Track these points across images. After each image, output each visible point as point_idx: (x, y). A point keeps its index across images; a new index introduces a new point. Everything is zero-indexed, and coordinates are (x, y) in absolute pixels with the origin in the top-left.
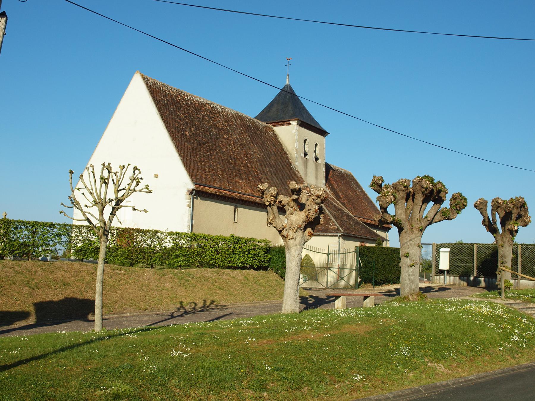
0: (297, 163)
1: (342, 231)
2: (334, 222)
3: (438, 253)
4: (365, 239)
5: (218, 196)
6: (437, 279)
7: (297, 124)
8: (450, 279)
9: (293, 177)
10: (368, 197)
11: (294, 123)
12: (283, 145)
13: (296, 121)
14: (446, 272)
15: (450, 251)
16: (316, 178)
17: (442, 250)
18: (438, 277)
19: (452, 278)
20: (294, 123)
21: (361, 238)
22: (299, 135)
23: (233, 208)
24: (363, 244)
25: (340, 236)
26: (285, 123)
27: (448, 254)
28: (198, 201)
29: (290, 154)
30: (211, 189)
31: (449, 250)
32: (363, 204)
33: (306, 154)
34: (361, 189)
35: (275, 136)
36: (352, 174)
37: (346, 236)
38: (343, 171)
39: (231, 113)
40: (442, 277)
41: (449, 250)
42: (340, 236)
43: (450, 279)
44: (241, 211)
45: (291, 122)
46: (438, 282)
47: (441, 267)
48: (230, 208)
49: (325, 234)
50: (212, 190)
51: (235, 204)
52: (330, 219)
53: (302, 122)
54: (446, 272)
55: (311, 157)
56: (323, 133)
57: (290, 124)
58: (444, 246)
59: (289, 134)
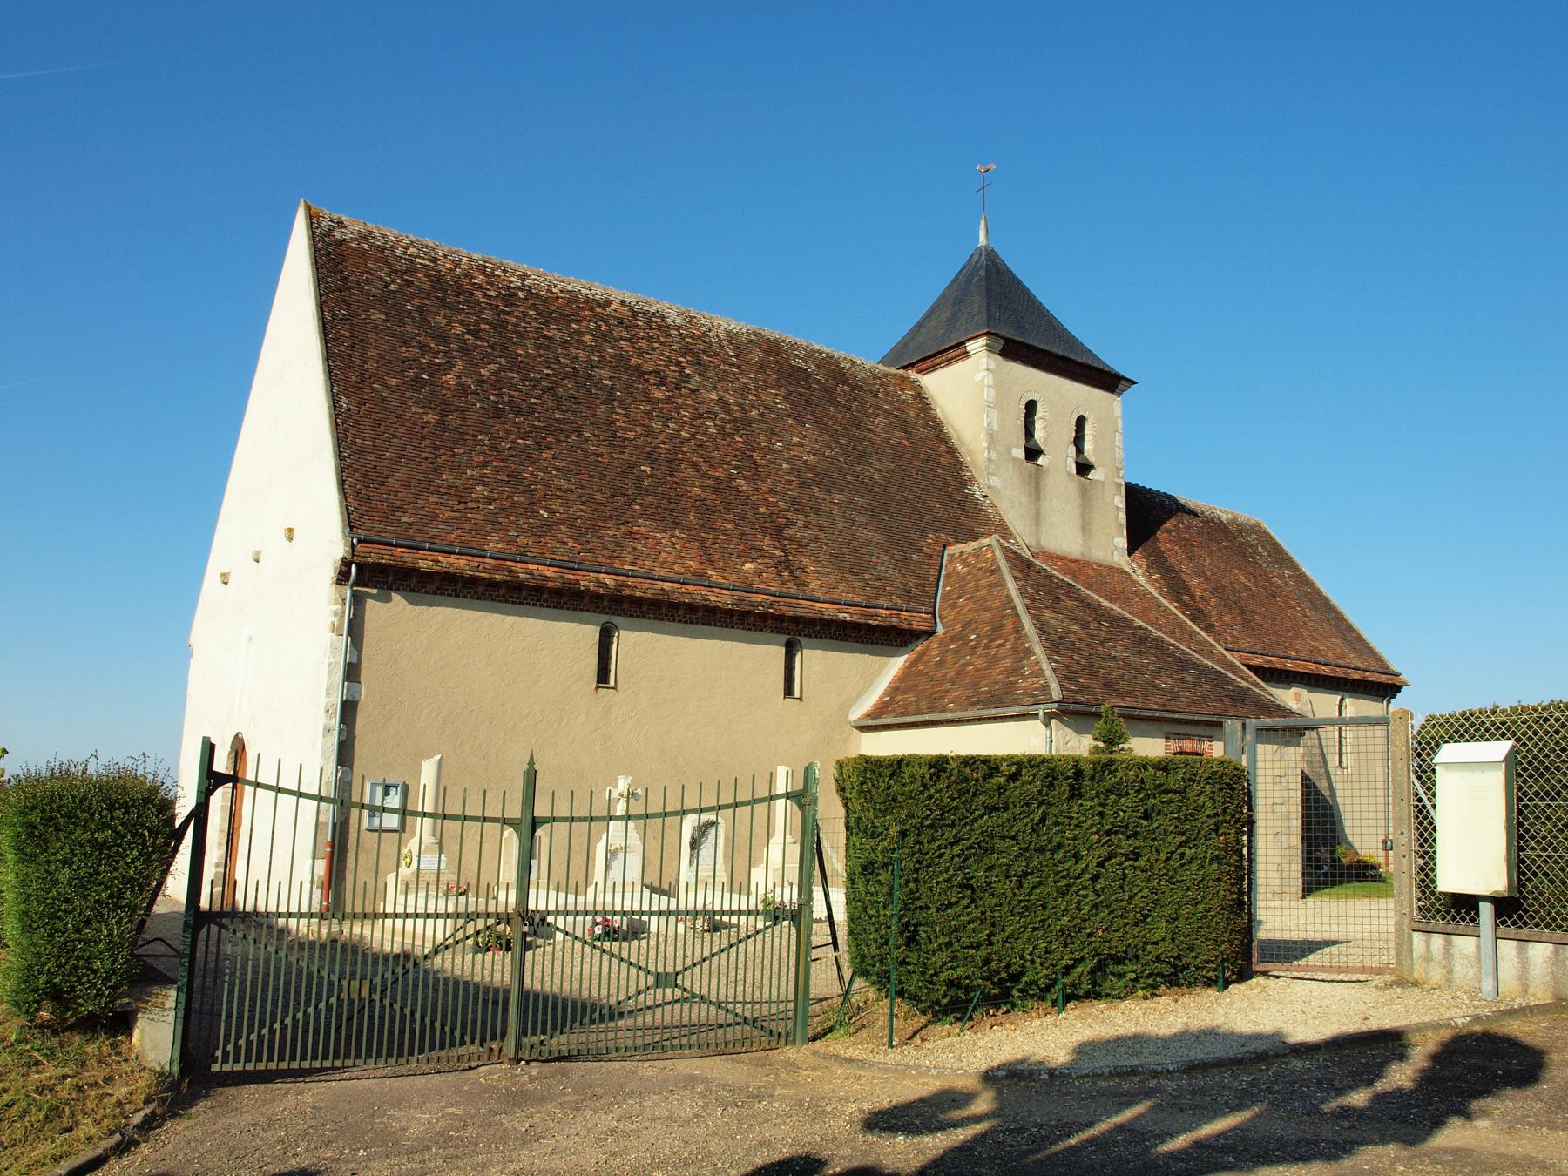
0: (995, 481)
1: (1056, 695)
2: (1037, 663)
3: (1426, 774)
4: (1197, 723)
5: (492, 585)
6: (1428, 958)
7: (990, 349)
8: (1524, 963)
9: (964, 521)
10: (1318, 592)
11: (977, 346)
12: (948, 429)
13: (983, 341)
14: (1486, 910)
15: (1511, 760)
16: (1086, 529)
17: (1448, 752)
18: (1437, 941)
19: (1540, 952)
20: (977, 346)
21: (1166, 720)
22: (999, 385)
23: (781, 651)
24: (1187, 745)
25: (1049, 716)
26: (952, 354)
27: (1498, 778)
28: (392, 615)
29: (970, 453)
30: (453, 559)
31: (1499, 749)
32: (1290, 612)
33: (1033, 453)
34: (1293, 566)
35: (923, 404)
36: (1264, 525)
37: (1073, 713)
38: (1224, 518)
39: (728, 333)
40: (1464, 945)
41: (1499, 749)
42: (1049, 716)
43: (1524, 963)
44: (632, 643)
45: (970, 346)
46: (1436, 975)
47: (1450, 880)
48: (580, 635)
49: (993, 712)
50: (460, 564)
51: (604, 618)
52: (1029, 652)
53: (1008, 341)
54: (1486, 910)
55: (1057, 458)
56: (1109, 381)
57: (966, 355)
58: (1470, 727)
59: (971, 395)
